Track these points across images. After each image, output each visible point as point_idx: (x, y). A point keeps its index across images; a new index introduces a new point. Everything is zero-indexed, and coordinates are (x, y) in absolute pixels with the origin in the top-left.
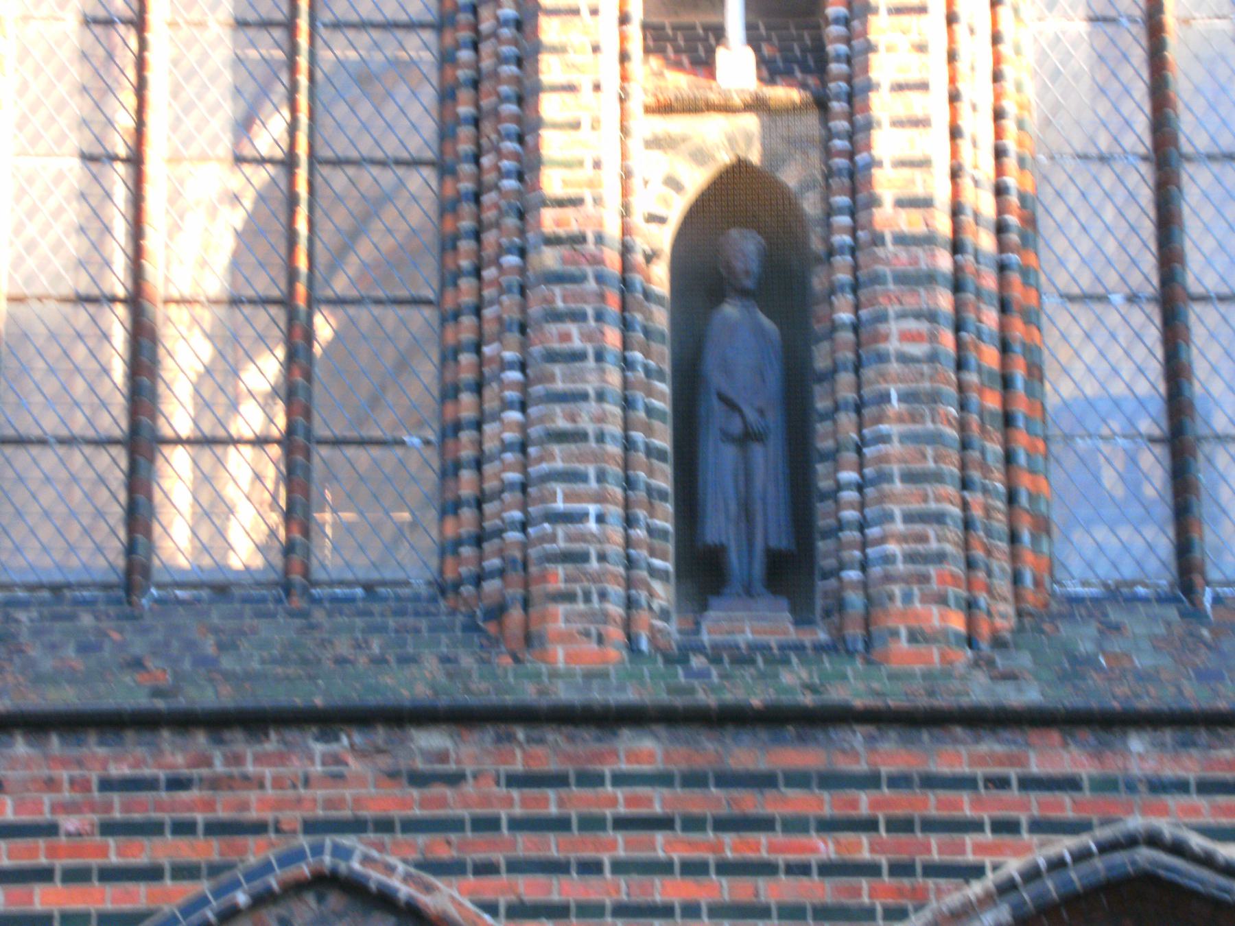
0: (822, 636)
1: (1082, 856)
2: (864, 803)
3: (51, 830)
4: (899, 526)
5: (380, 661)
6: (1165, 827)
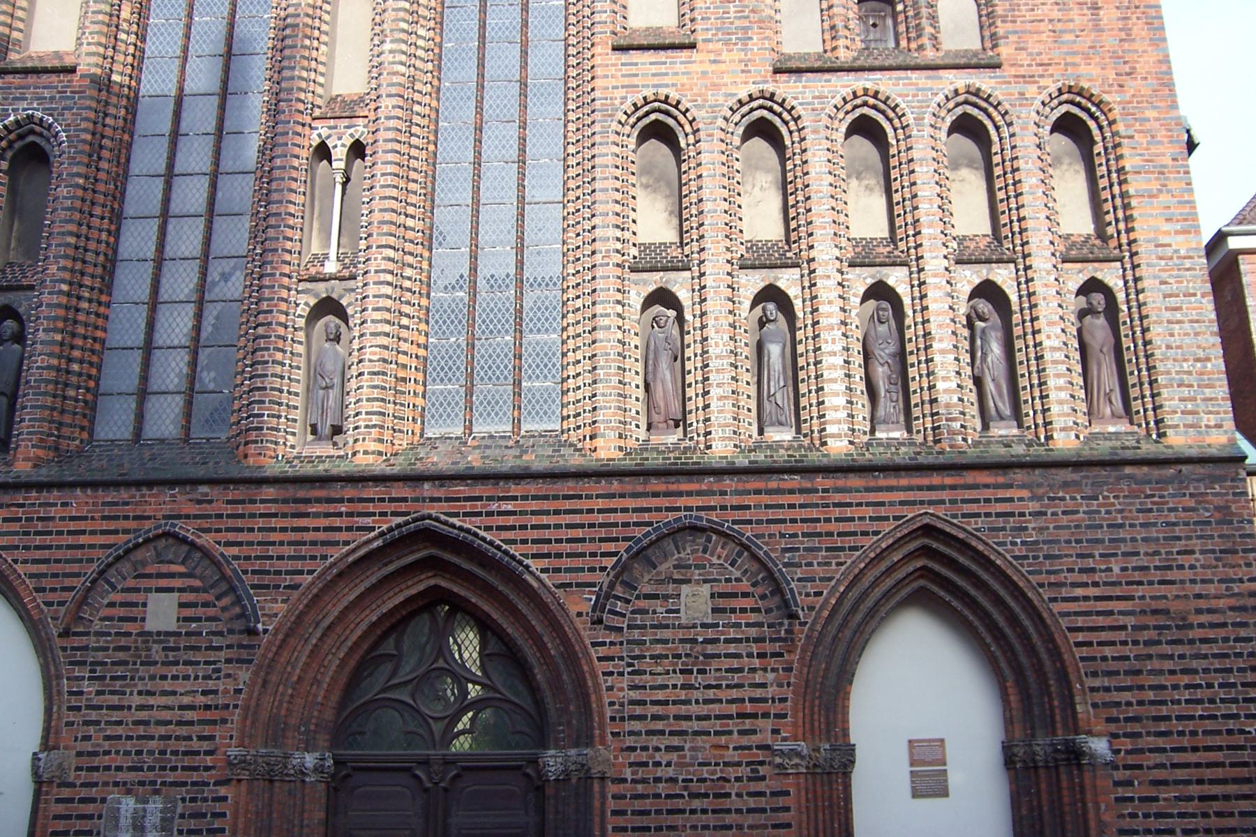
6: (433, 512)
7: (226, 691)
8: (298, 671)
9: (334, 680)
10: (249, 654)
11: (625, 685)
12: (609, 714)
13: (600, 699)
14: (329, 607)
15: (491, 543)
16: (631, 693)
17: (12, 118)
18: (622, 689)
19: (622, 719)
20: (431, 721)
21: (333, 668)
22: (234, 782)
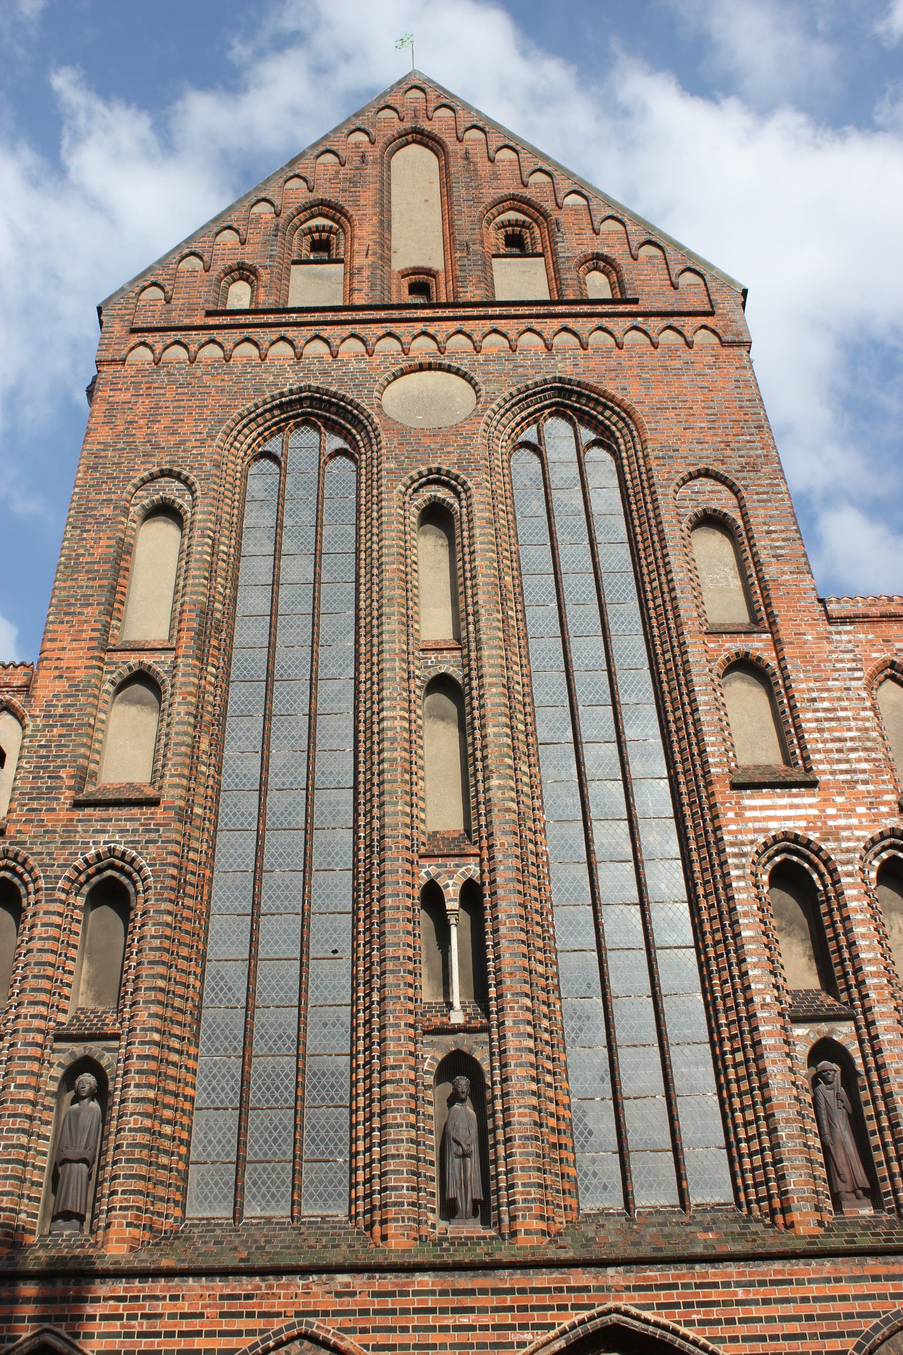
0: (493, 1233)
1: (592, 1318)
2: (508, 1300)
3: (201, 1315)
4: (520, 1189)
5: (325, 1247)
17: (93, 851)
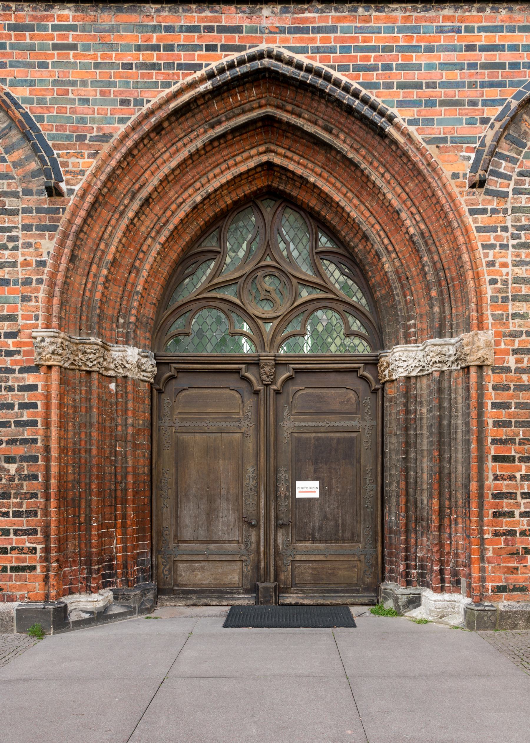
6: (276, 48)
7: (26, 264)
8: (113, 249)
9: (153, 273)
10: (51, 219)
11: (509, 260)
12: (489, 294)
13: (477, 277)
14: (147, 175)
15: (346, 89)
16: (516, 269)
18: (504, 265)
19: (505, 299)
20: (260, 322)
21: (154, 253)
22: (43, 370)
